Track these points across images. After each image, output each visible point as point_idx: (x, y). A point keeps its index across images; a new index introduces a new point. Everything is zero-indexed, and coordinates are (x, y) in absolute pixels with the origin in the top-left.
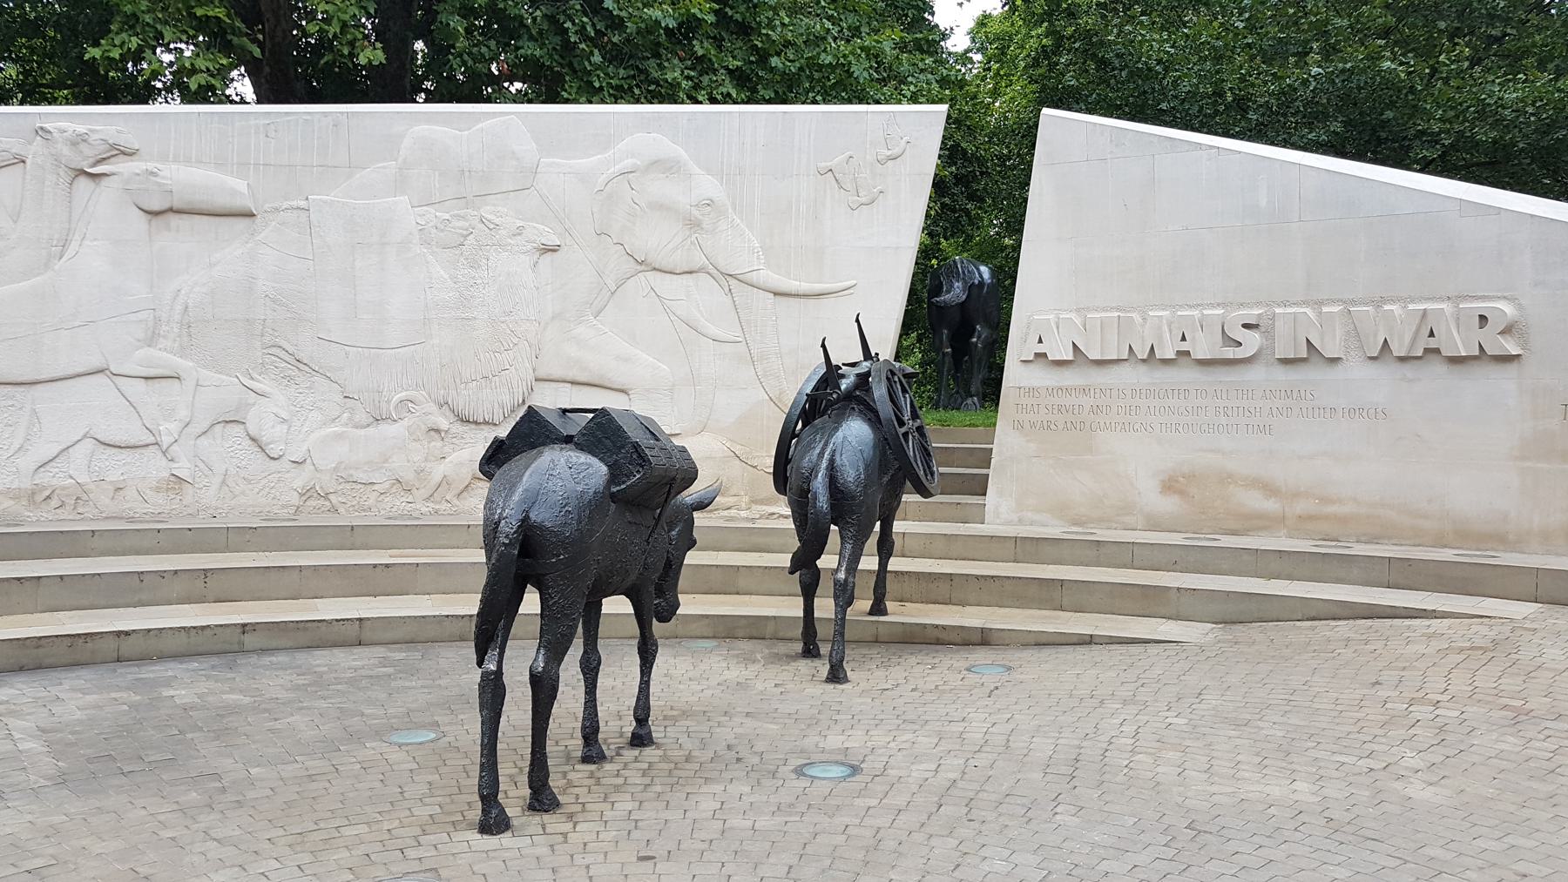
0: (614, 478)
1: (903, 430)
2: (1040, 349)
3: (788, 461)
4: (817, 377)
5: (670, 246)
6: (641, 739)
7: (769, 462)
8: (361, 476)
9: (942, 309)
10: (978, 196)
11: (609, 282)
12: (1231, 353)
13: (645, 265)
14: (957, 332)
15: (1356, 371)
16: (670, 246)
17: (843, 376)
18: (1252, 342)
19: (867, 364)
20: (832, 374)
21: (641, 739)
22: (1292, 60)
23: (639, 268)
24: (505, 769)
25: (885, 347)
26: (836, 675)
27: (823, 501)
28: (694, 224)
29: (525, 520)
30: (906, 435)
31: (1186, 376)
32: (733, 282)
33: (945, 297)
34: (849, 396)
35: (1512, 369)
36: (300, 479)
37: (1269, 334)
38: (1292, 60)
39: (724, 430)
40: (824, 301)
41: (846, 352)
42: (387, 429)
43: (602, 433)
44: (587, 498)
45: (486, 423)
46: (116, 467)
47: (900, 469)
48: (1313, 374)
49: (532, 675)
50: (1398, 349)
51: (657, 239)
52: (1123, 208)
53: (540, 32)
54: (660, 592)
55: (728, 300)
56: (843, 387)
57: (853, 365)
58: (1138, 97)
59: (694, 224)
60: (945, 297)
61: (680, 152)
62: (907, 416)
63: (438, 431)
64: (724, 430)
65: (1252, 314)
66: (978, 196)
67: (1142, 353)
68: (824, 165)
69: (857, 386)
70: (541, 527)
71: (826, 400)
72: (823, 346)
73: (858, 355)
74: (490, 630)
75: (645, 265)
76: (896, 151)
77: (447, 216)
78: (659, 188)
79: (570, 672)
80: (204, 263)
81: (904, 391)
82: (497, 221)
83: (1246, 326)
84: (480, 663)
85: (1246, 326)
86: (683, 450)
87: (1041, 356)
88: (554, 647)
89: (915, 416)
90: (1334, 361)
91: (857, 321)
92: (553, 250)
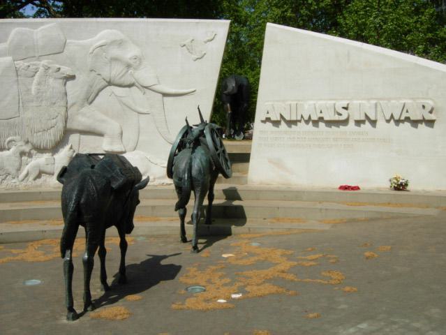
3: (173, 165)
5: (121, 75)
7: (166, 164)
10: (241, 67)
14: (236, 104)
25: (207, 118)
30: (219, 154)
39: (151, 161)
41: (194, 121)
45: (52, 127)
47: (218, 166)
51: (115, 72)
52: (296, 61)
53: (130, 314)
57: (197, 126)
58: (326, 21)
59: (129, 66)
62: (219, 147)
64: (151, 161)
66: (241, 67)
72: (198, 108)
74: (67, 243)
78: (115, 52)
79: (97, 258)
84: (63, 256)
88: (91, 252)
91: (198, 108)
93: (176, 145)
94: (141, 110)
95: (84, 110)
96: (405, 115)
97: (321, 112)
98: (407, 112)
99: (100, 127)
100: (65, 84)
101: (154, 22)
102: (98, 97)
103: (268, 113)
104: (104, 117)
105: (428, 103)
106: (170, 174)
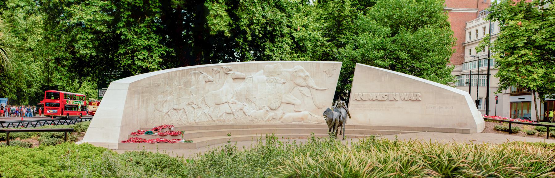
10: (346, 79)
12: (383, 99)
15: (400, 102)
18: (386, 98)
22: (410, 30)
28: (305, 79)
31: (376, 102)
35: (419, 102)
36: (250, 118)
37: (389, 96)
38: (410, 30)
42: (261, 111)
46: (228, 117)
48: (394, 102)
51: (299, 81)
55: (126, 140)
61: (303, 68)
65: (387, 94)
66: (346, 79)
78: (302, 74)
80: (240, 86)
87: (356, 99)
104: (295, 98)
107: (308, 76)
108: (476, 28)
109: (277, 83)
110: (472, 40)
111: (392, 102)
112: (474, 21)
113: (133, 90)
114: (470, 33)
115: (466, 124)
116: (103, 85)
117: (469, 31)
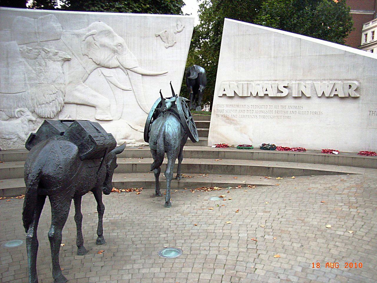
0: (80, 151)
1: (187, 120)
2: (224, 93)
4: (158, 103)
5: (107, 60)
6: (100, 240)
8: (7, 137)
9: (190, 80)
10: (206, 49)
11: (88, 71)
12: (279, 95)
13: (100, 65)
14: (198, 88)
16: (107, 60)
17: (167, 103)
19: (174, 98)
20: (162, 104)
21: (100, 240)
23: (97, 66)
24: (49, 259)
25: (177, 91)
26: (168, 204)
27: (162, 147)
28: (115, 52)
29: (40, 173)
30: (188, 122)
31: (267, 102)
32: (128, 71)
33: (191, 77)
34: (169, 110)
40: (158, 77)
43: (77, 132)
44: (68, 161)
48: (303, 101)
49: (49, 237)
50: (327, 95)
51: (102, 56)
54: (105, 184)
56: (167, 106)
57: (169, 98)
58: (249, 16)
59: (115, 52)
60: (191, 77)
63: (32, 121)
66: (206, 49)
67: (254, 95)
68: (158, 33)
69: (172, 106)
70: (48, 176)
71: (160, 111)
72: (160, 92)
73: (171, 95)
75: (100, 65)
76: (179, 30)
77: (31, 48)
78: (106, 40)
81: (186, 107)
82: (49, 50)
83: (284, 87)
85: (284, 87)
86: (110, 135)
87: (224, 95)
89: (190, 115)
90: (309, 98)
91: (160, 92)
92: (68, 60)
93: (152, 114)
94: (125, 88)
95: (79, 87)
96: (334, 93)
97: (266, 90)
98: (336, 90)
99: (93, 102)
100: (63, 65)
101: (157, 17)
102: (114, 69)
103: (224, 90)
104: (95, 93)
105: (353, 84)
106: (147, 138)
107: (120, 45)
108: (372, 30)
109: (50, 58)
110: (368, 42)
111: (298, 101)
112: (371, 23)
113: (217, 142)
114: (366, 35)
115: (178, 127)
116: (58, 117)
117: (366, 33)
